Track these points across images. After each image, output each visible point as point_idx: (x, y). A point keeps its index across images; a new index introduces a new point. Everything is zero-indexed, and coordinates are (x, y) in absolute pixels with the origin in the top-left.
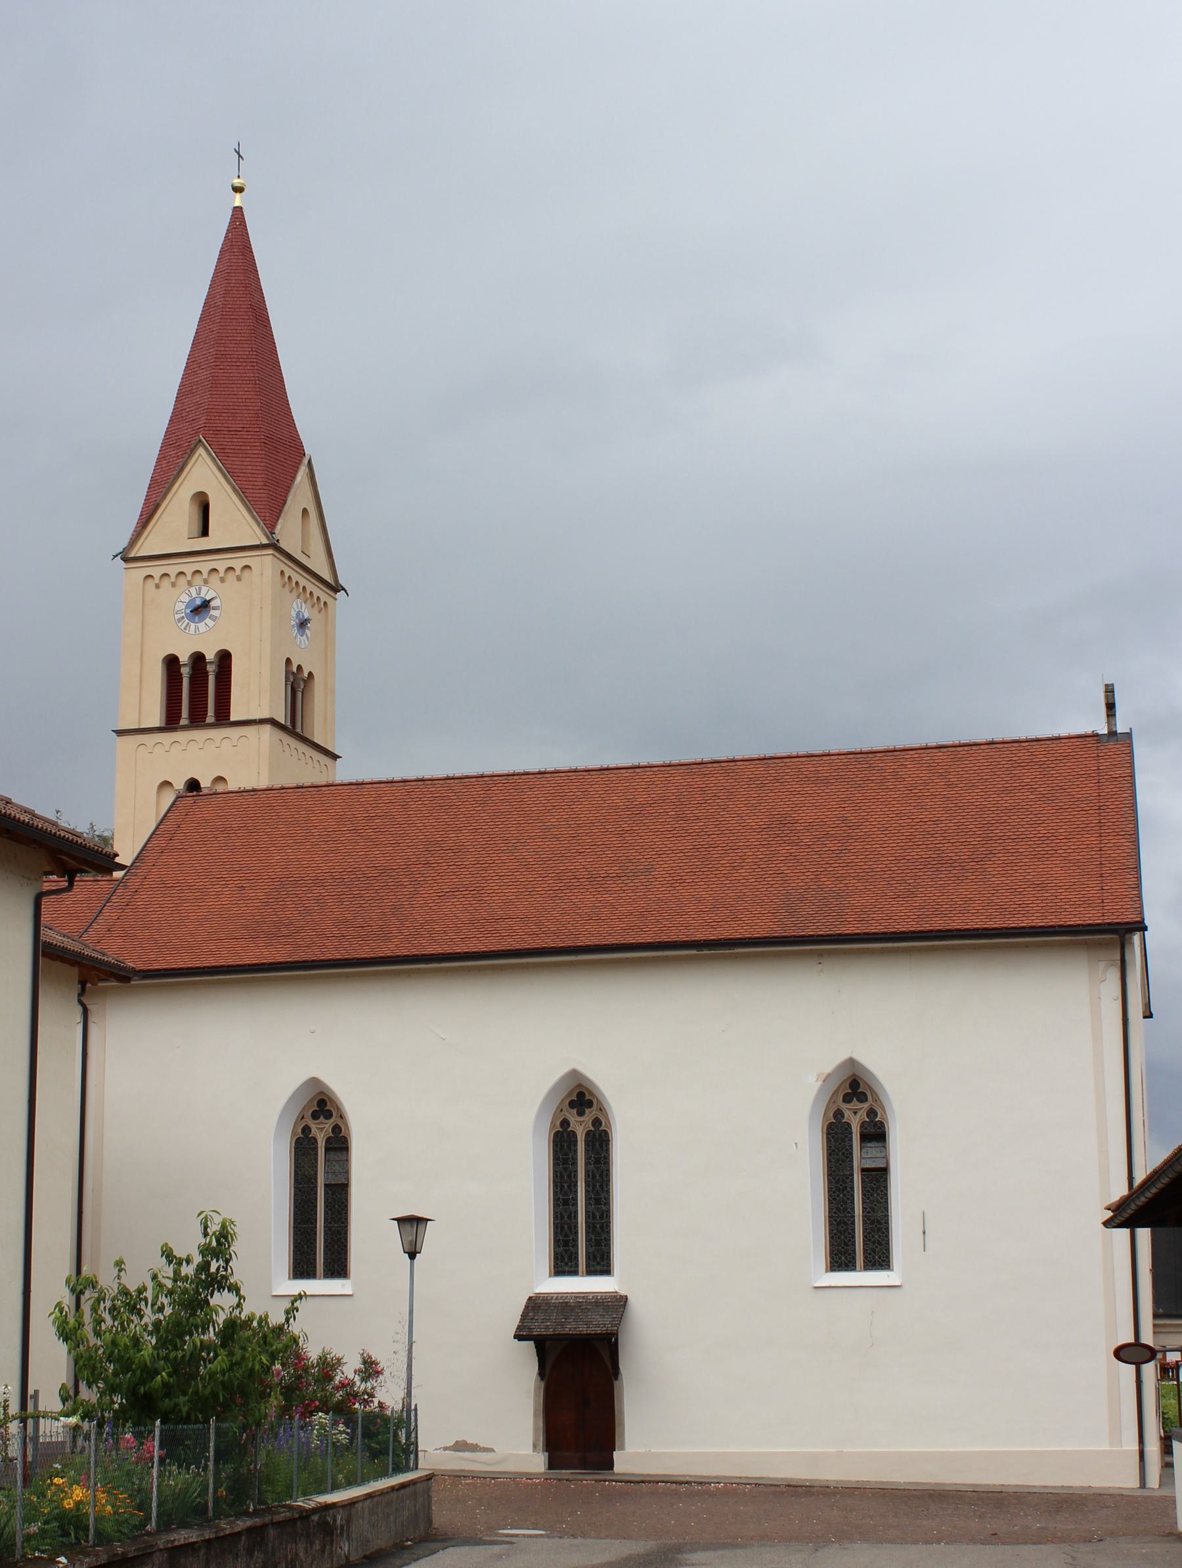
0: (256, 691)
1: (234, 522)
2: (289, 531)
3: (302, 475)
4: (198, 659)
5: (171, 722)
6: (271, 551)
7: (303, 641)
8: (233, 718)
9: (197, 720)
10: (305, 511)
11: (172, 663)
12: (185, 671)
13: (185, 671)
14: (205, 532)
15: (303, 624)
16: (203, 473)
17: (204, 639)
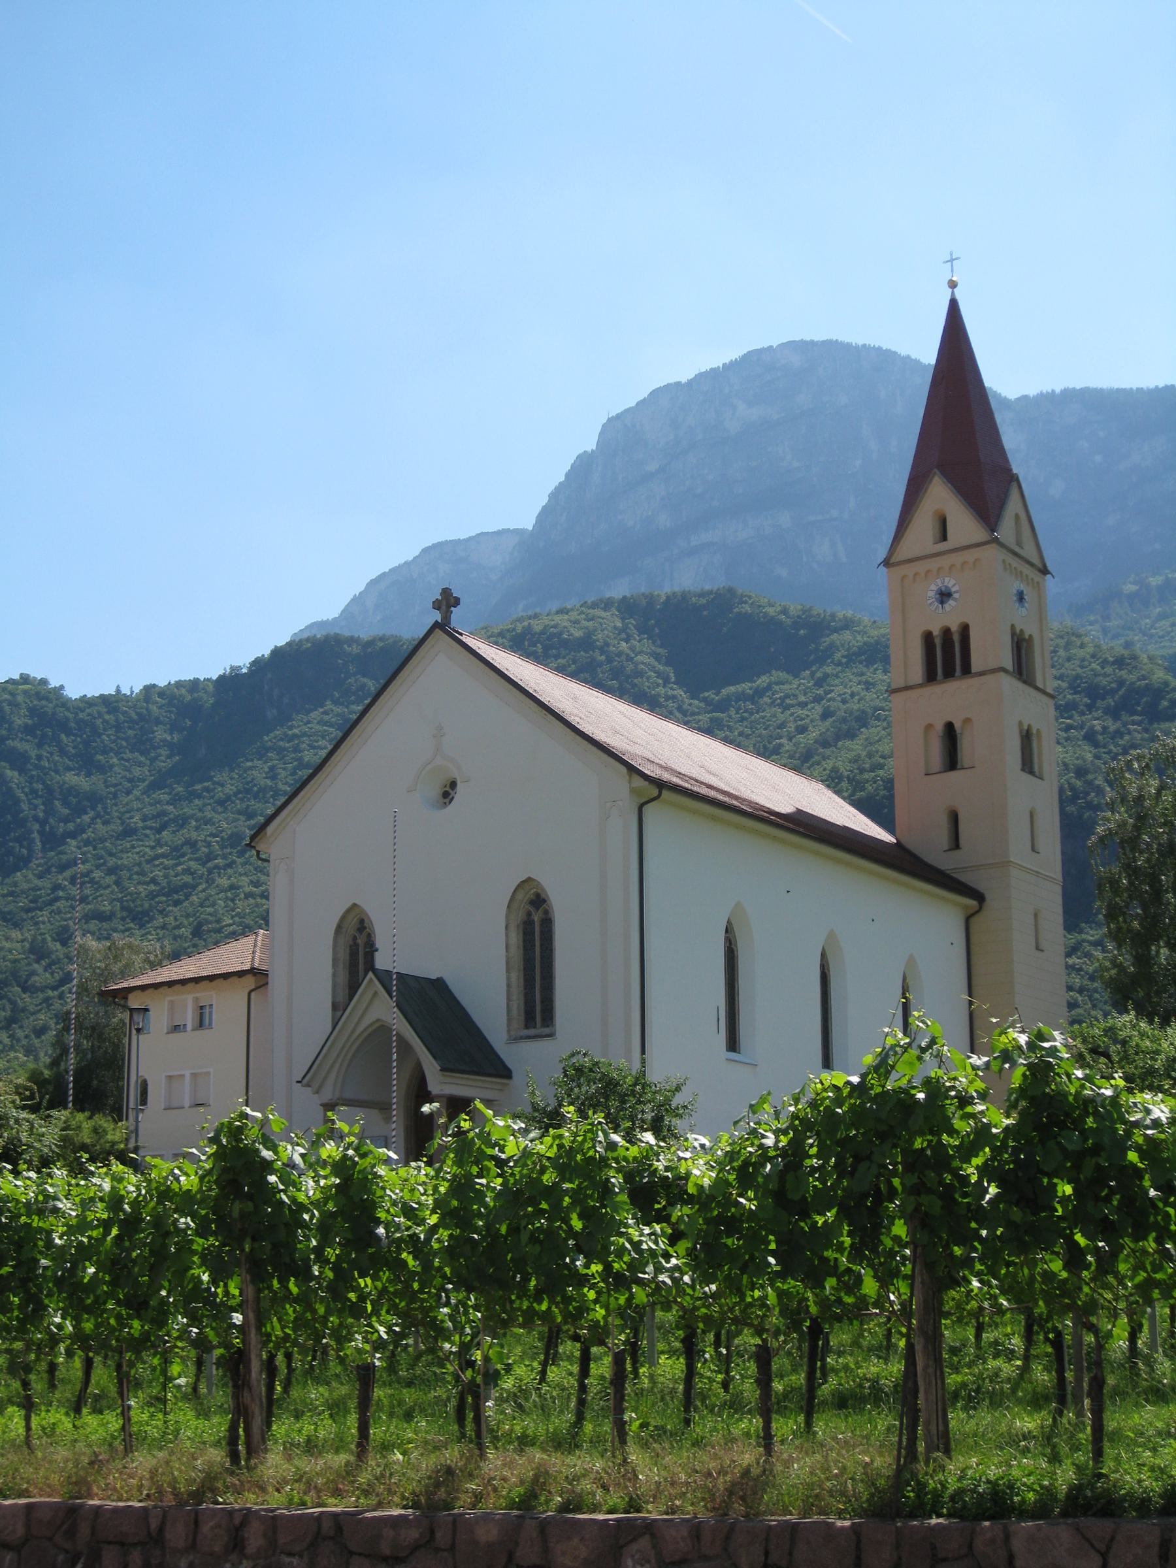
0: (991, 649)
1: (965, 526)
2: (1006, 531)
3: (1014, 494)
4: (947, 632)
5: (931, 677)
6: (994, 545)
7: (1023, 612)
8: (973, 670)
9: (949, 674)
10: (1017, 516)
11: (928, 637)
12: (938, 642)
13: (938, 642)
14: (944, 537)
15: (1021, 597)
16: (940, 495)
17: (950, 617)
